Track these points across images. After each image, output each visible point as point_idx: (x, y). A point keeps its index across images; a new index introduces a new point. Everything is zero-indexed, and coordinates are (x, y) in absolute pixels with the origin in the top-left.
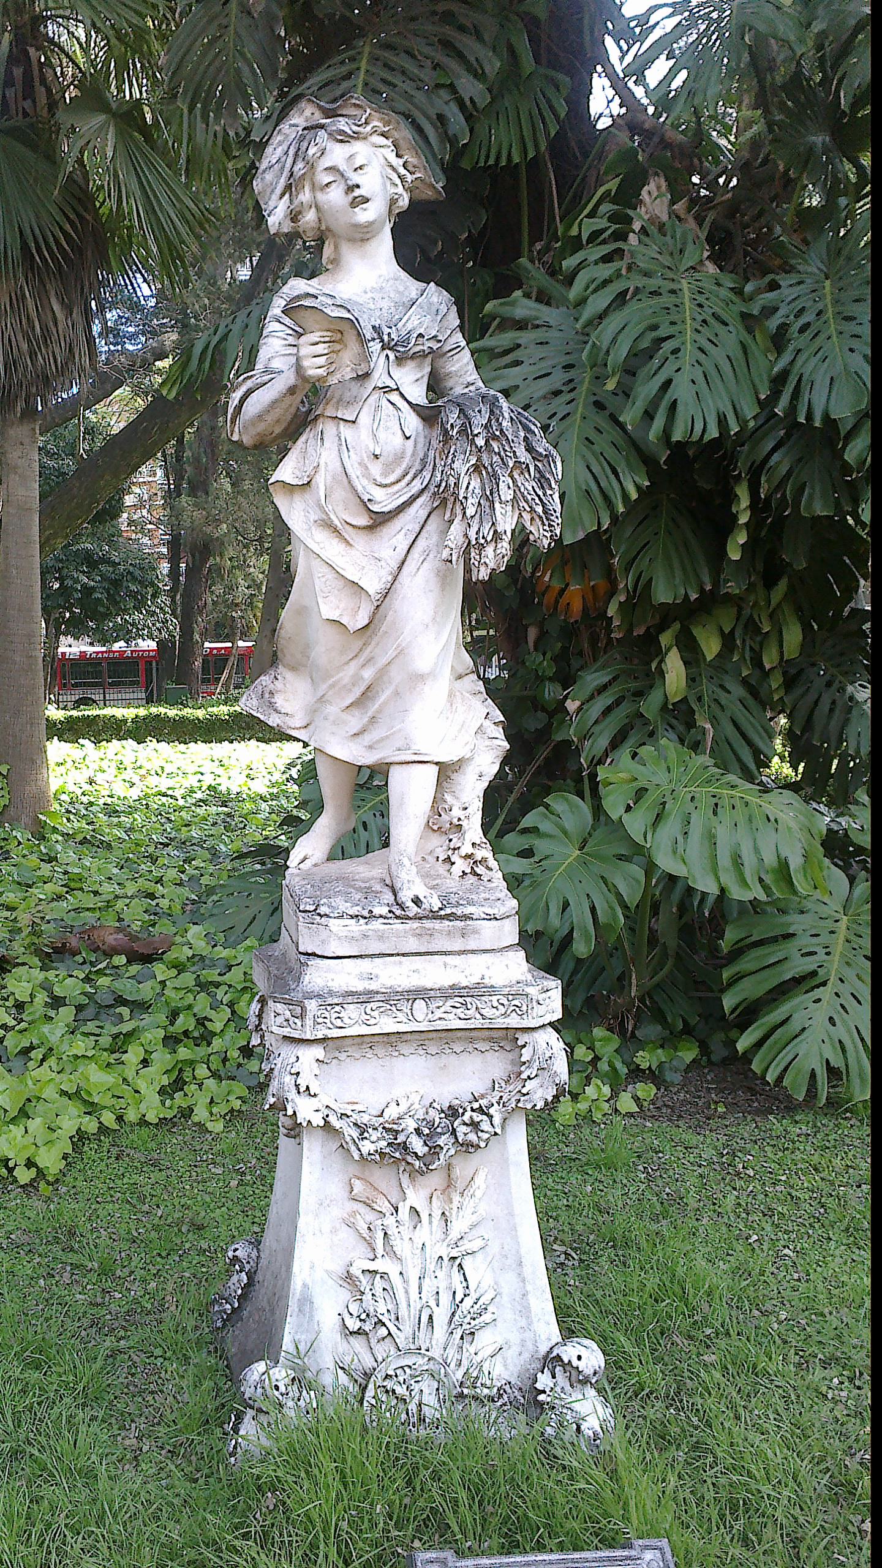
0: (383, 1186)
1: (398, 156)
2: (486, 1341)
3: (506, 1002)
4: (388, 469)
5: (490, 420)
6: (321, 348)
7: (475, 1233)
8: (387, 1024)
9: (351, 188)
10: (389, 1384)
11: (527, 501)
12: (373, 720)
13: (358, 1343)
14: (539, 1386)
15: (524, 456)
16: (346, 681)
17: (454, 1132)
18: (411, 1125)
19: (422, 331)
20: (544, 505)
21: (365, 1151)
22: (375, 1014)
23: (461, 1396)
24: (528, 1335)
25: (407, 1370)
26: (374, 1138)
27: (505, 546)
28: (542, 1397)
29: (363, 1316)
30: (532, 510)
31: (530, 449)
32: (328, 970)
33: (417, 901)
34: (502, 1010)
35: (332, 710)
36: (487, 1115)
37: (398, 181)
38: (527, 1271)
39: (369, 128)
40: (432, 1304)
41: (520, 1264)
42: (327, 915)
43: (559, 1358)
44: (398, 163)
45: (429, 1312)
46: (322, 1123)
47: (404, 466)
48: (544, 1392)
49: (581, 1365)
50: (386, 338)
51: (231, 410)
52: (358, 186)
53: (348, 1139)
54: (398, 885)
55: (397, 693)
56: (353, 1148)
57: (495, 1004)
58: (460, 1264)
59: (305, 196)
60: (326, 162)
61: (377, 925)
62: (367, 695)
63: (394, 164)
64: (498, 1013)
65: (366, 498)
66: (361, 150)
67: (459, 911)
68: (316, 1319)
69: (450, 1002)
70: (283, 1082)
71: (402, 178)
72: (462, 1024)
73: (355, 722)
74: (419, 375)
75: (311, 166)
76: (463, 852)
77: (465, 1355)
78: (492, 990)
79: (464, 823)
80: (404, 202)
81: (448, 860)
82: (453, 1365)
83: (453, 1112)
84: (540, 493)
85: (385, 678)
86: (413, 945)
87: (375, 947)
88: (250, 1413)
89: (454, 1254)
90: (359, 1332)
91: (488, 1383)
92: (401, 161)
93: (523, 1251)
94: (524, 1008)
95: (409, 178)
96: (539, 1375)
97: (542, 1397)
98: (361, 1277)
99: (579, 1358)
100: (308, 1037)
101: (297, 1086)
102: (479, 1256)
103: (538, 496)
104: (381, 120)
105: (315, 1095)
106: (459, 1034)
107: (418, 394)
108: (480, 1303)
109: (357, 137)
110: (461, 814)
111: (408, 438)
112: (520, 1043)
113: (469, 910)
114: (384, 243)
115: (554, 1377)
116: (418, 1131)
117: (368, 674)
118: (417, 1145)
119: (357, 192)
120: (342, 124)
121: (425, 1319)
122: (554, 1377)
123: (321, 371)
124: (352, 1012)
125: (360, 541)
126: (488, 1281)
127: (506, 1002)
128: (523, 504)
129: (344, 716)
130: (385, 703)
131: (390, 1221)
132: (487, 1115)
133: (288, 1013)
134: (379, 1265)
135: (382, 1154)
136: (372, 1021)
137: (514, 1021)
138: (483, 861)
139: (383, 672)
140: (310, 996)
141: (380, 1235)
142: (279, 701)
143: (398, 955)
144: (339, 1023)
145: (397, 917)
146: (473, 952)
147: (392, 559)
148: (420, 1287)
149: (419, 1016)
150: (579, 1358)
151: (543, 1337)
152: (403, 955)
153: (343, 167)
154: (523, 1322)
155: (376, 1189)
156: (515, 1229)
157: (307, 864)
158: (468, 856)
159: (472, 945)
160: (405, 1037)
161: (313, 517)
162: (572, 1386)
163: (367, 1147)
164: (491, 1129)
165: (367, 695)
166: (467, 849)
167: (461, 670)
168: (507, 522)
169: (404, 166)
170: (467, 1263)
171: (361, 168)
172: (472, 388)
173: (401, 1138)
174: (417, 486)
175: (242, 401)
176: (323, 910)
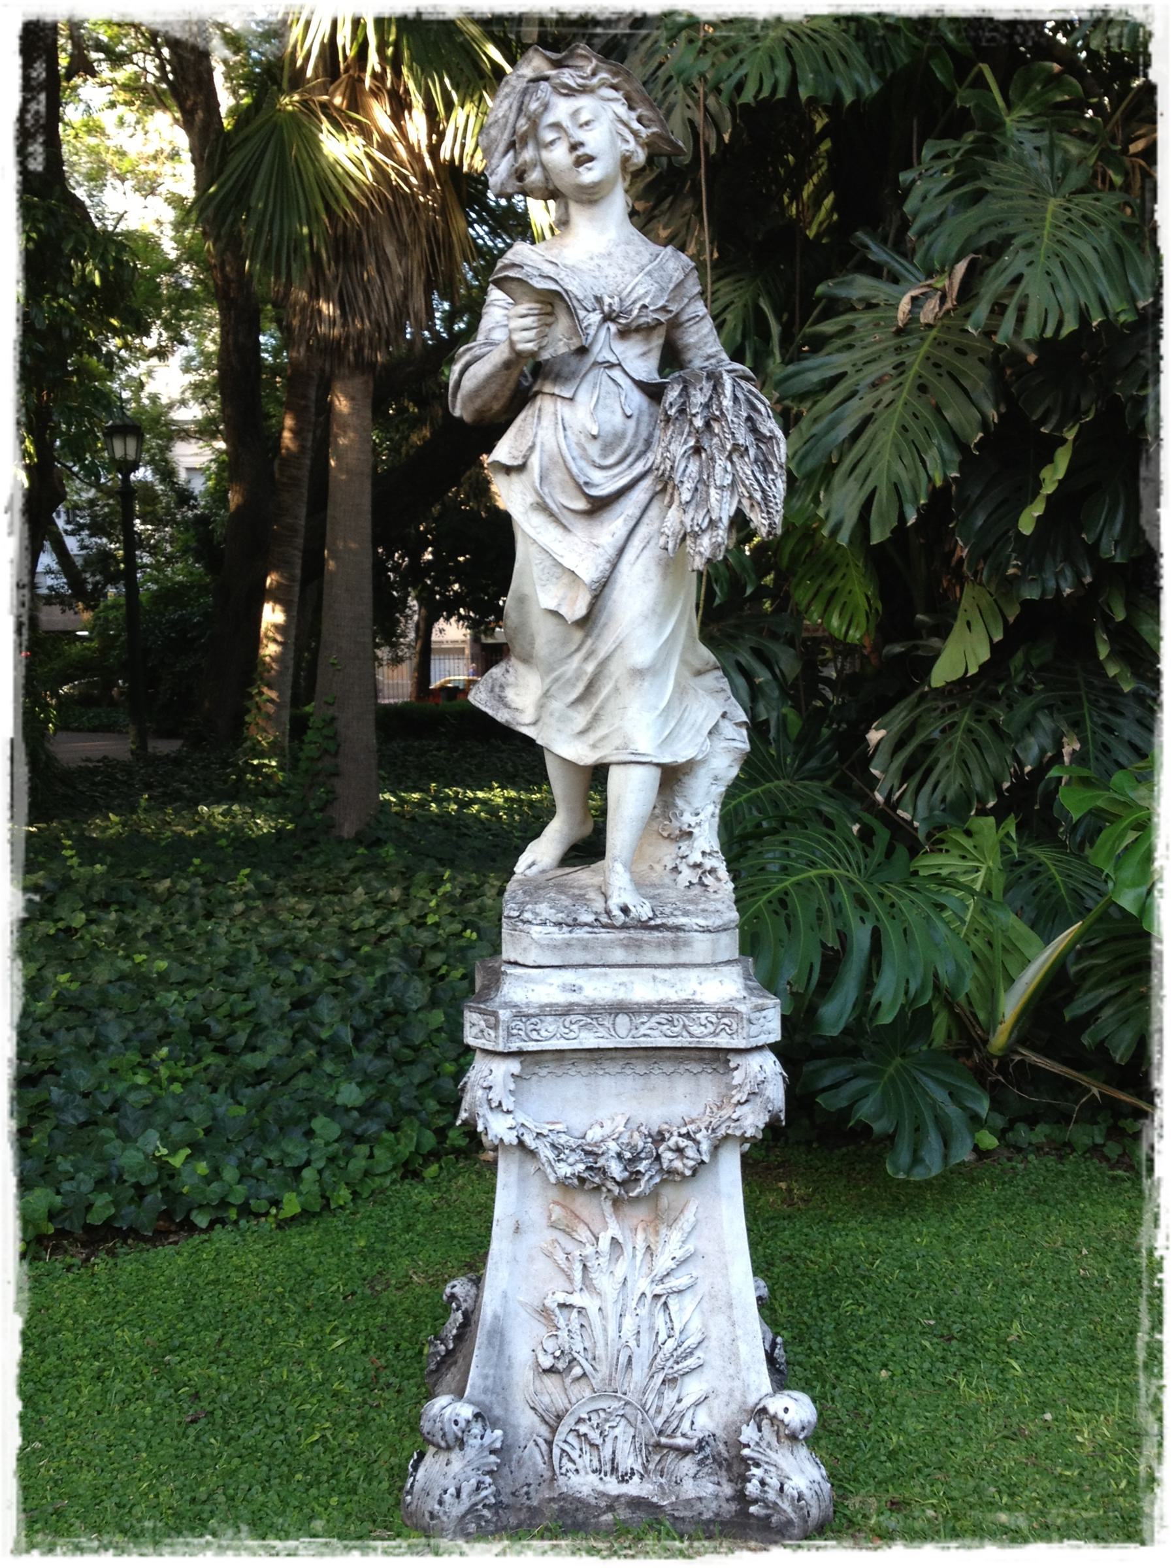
0: (584, 1213)
1: (631, 108)
2: (693, 1388)
3: (714, 1020)
4: (607, 449)
5: (711, 398)
6: (528, 321)
7: (683, 1270)
8: (589, 1040)
10: (583, 1429)
11: (744, 486)
12: (596, 717)
13: (551, 1382)
14: (743, 1439)
15: (743, 437)
16: (569, 674)
17: (658, 1158)
18: (613, 1147)
19: (647, 301)
20: (763, 491)
22: (574, 1027)
23: (658, 1445)
24: (737, 1383)
25: (602, 1414)
27: (721, 534)
29: (558, 1353)
30: (751, 497)
31: (754, 430)
32: (530, 980)
33: (625, 910)
34: (711, 1028)
35: (557, 705)
36: (694, 1140)
37: (630, 137)
38: (737, 1314)
39: (595, 81)
40: (633, 1343)
41: (730, 1306)
42: (529, 922)
43: (764, 1410)
44: (631, 117)
45: (628, 1352)
46: (515, 1142)
47: (625, 446)
48: (748, 1446)
49: (787, 1418)
50: (606, 309)
51: (451, 383)
52: (582, 144)
53: (544, 1160)
54: (609, 893)
55: (616, 689)
56: (549, 1170)
57: (704, 1022)
58: (665, 1303)
61: (580, 933)
62: (590, 689)
63: (625, 117)
64: (706, 1031)
67: (671, 921)
68: (507, 1353)
69: (656, 1018)
70: (473, 1096)
71: (635, 134)
72: (666, 1043)
73: (581, 718)
74: (645, 349)
76: (691, 861)
77: (666, 1402)
78: (700, 1007)
79: (696, 831)
80: (641, 157)
81: (675, 869)
82: (652, 1412)
83: (659, 1138)
84: (761, 478)
85: (606, 672)
86: (619, 955)
87: (578, 957)
88: (431, 1450)
89: (658, 1290)
90: (551, 1370)
91: (690, 1433)
92: (634, 115)
93: (734, 1292)
94: (734, 1027)
95: (644, 132)
96: (744, 1427)
97: (746, 1452)
98: (557, 1311)
99: (786, 1410)
100: (500, 1048)
101: (489, 1101)
102: (688, 1297)
103: (757, 481)
104: (609, 71)
105: (509, 1112)
106: (668, 1053)
107: (645, 368)
108: (685, 1345)
109: (584, 90)
110: (693, 820)
111: (629, 417)
113: (682, 920)
114: (618, 203)
115: (760, 1430)
116: (619, 1156)
117: (590, 668)
118: (616, 1170)
119: (581, 151)
120: (568, 77)
121: (623, 1359)
122: (760, 1430)
124: (550, 1026)
125: (580, 527)
126: (695, 1325)
127: (714, 1020)
128: (742, 489)
129: (572, 713)
130: (607, 699)
131: (589, 1250)
132: (694, 1140)
133: (483, 1023)
134: (576, 1300)
135: (582, 1180)
136: (572, 1035)
137: (723, 1041)
138: (712, 871)
139: (603, 664)
140: (507, 1005)
141: (578, 1267)
142: (510, 694)
143: (604, 966)
144: (534, 1035)
145: (604, 926)
146: (684, 965)
148: (620, 1326)
149: (622, 1031)
150: (786, 1410)
151: (752, 1388)
152: (610, 966)
153: (566, 123)
154: (731, 1370)
155: (577, 1217)
156: (726, 1267)
157: (535, 869)
158: (697, 866)
159: (684, 958)
160: (610, 1054)
162: (779, 1441)
163: (564, 1170)
164: (697, 1156)
165: (590, 689)
166: (696, 857)
167: (698, 665)
168: (724, 508)
169: (639, 120)
170: (673, 1303)
171: (587, 123)
172: (713, 361)
174: (639, 468)
176: (527, 916)
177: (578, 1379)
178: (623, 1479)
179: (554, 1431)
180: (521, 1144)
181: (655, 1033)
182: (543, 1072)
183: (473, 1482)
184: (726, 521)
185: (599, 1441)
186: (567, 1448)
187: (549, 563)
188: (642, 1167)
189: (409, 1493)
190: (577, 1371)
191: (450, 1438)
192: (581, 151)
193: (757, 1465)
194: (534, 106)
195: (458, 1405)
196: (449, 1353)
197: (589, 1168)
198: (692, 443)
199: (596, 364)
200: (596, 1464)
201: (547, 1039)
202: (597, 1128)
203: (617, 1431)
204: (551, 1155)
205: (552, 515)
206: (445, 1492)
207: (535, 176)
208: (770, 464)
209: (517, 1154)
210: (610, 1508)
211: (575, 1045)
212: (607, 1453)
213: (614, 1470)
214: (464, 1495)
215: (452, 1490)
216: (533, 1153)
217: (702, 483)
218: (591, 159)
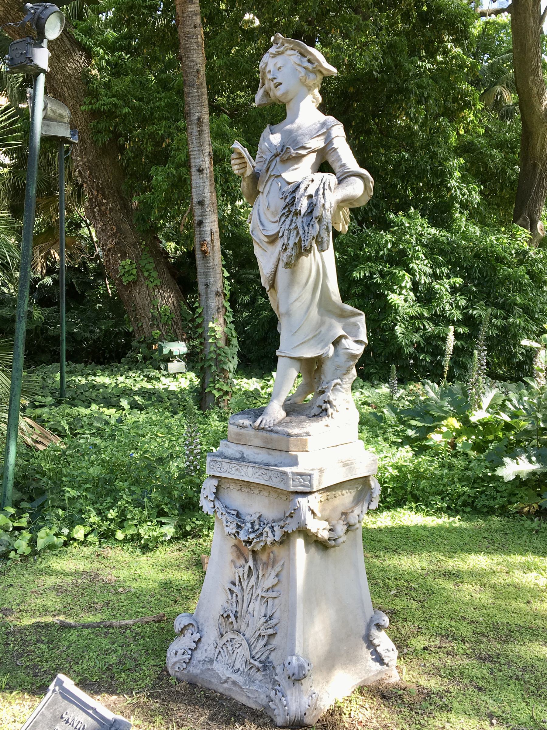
150: (289, 663)
186: (221, 651)
202: (249, 516)
210: (226, 681)
218: (280, 84)
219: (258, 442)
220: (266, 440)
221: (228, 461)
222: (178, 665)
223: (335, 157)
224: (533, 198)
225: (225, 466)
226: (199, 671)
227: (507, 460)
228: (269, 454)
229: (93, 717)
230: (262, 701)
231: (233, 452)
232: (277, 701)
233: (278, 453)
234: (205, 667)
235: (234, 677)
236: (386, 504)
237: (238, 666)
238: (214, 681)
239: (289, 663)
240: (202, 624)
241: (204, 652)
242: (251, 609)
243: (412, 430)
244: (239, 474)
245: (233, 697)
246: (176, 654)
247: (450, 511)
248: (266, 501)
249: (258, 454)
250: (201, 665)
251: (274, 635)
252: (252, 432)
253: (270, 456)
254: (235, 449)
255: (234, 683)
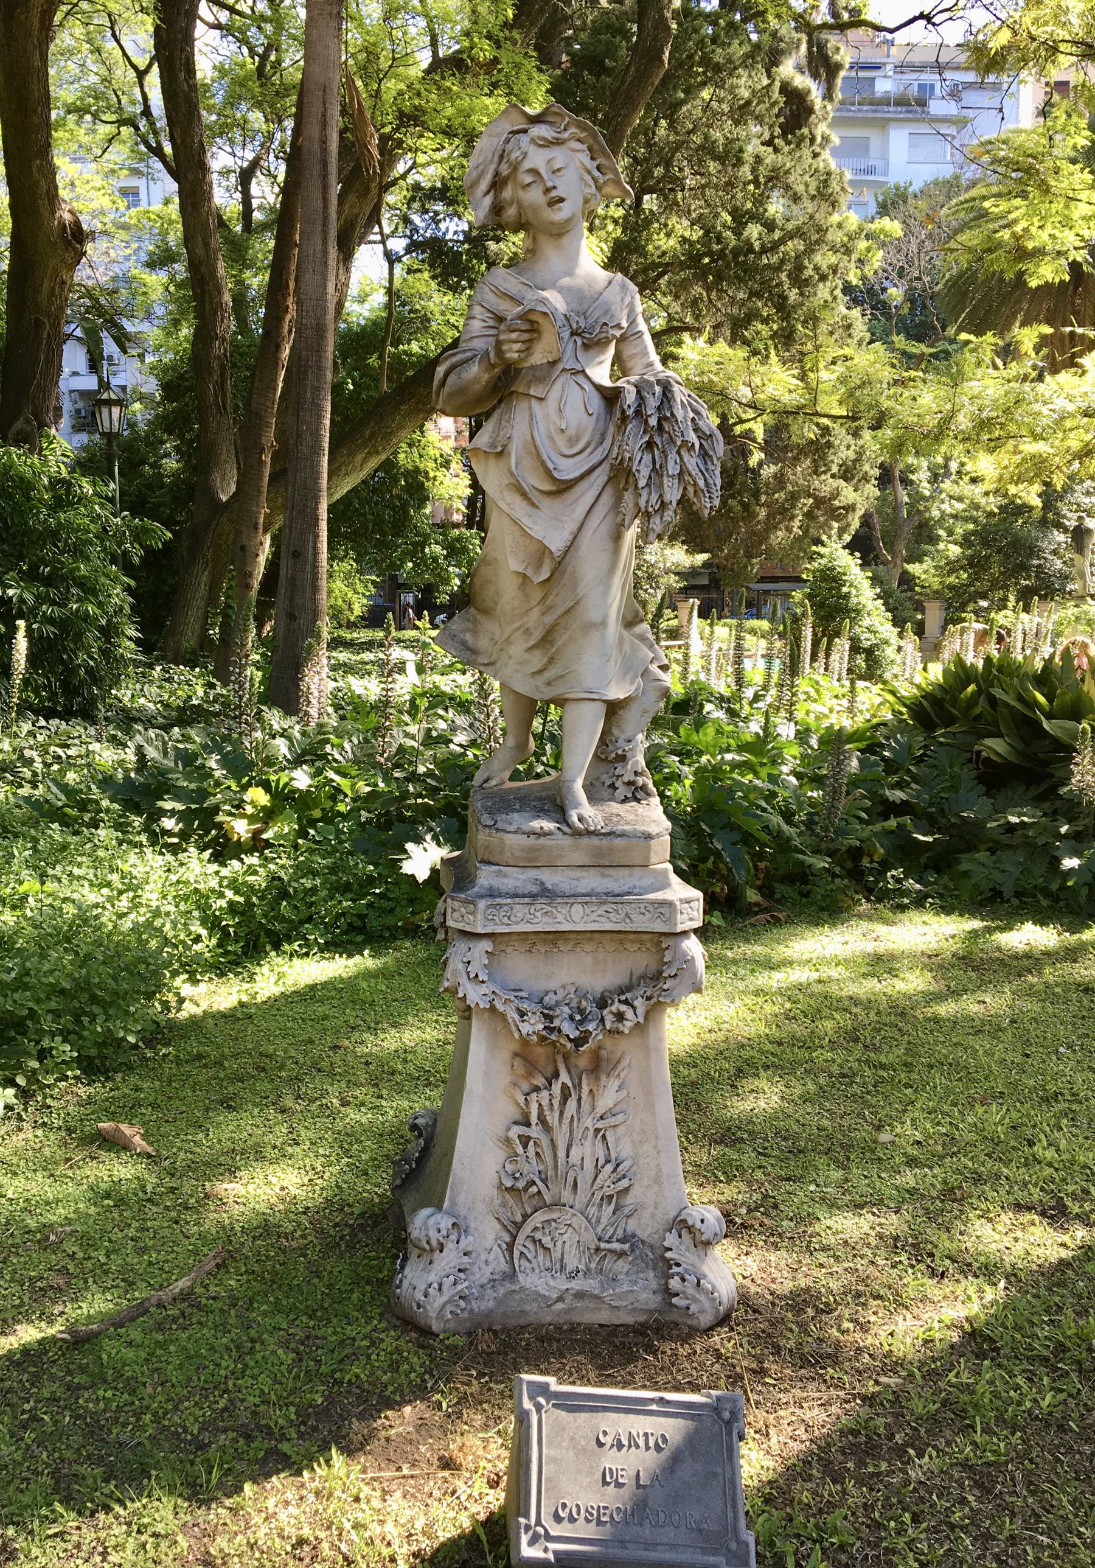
1: (592, 158)
9: (548, 190)
14: (666, 1244)
21: (524, 1031)
22: (538, 914)
26: (532, 1021)
28: (668, 1255)
30: (695, 484)
43: (684, 1221)
50: (575, 326)
51: (436, 382)
59: (507, 193)
60: (527, 165)
63: (589, 167)
65: (551, 466)
66: (559, 156)
69: (604, 907)
75: (515, 167)
76: (626, 779)
89: (599, 1125)
97: (668, 1255)
100: (480, 930)
101: (468, 973)
109: (558, 142)
112: (664, 946)
119: (554, 194)
123: (516, 355)
125: (546, 503)
147: (571, 526)
149: (576, 918)
150: (702, 1221)
158: (630, 783)
161: (506, 481)
169: (598, 168)
171: (559, 170)
173: (556, 1023)
175: (447, 374)
177: (533, 1196)
178: (571, 1277)
179: (514, 1238)
180: (493, 1009)
181: (602, 919)
182: (509, 950)
183: (452, 1278)
184: (674, 504)
185: (550, 1246)
186: (525, 1251)
187: (517, 533)
188: (591, 1027)
189: (398, 1287)
190: (534, 1189)
191: (434, 1243)
192: (554, 194)
193: (678, 1265)
194: (516, 154)
195: (438, 1216)
196: (412, 1170)
197: (545, 1028)
198: (646, 438)
199: (564, 370)
200: (548, 1264)
201: (516, 923)
202: (552, 995)
203: (565, 1238)
204: (517, 1017)
205: (524, 495)
206: (430, 1286)
207: (511, 212)
208: (711, 457)
209: (486, 1015)
210: (560, 1299)
211: (539, 928)
212: (556, 1255)
213: (563, 1267)
214: (445, 1288)
215: (436, 1285)
216: (503, 1016)
217: (657, 472)
218: (561, 200)
219: (579, 858)
220: (599, 853)
221: (527, 900)
222: (449, 1308)
223: (638, 349)
224: (39, 384)
225: (520, 911)
226: (491, 1304)
227: (410, 846)
228: (603, 876)
229: (666, 1414)
230: (647, 1303)
231: (518, 883)
232: (690, 1291)
233: (625, 871)
234: (502, 1291)
235: (576, 1285)
236: (231, 957)
237: (572, 1263)
238: (532, 1307)
239: (702, 1221)
240: (465, 1218)
241: (483, 1266)
242: (575, 1156)
243: (170, 818)
244: (550, 920)
245: (578, 1320)
246: (440, 1289)
247: (336, 946)
248: (588, 960)
249: (578, 879)
250: (489, 1291)
251: (626, 1190)
252: (566, 841)
253: (606, 880)
254: (522, 877)
255: (580, 1295)
